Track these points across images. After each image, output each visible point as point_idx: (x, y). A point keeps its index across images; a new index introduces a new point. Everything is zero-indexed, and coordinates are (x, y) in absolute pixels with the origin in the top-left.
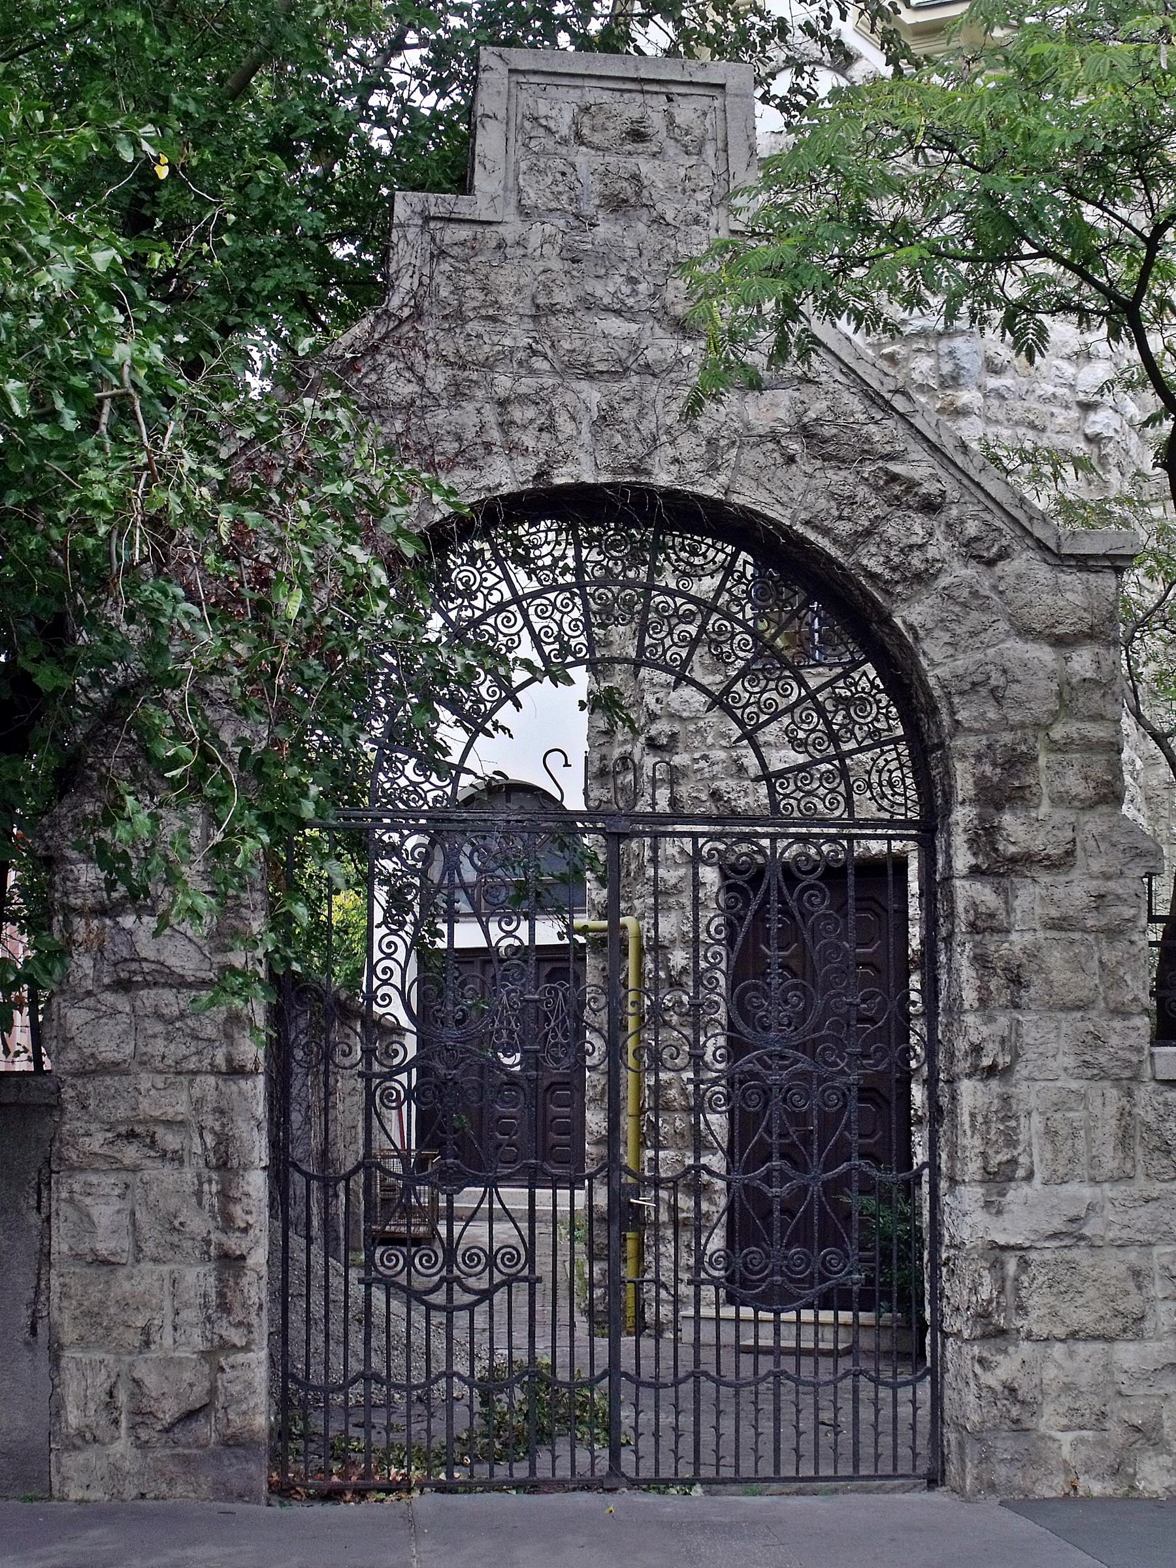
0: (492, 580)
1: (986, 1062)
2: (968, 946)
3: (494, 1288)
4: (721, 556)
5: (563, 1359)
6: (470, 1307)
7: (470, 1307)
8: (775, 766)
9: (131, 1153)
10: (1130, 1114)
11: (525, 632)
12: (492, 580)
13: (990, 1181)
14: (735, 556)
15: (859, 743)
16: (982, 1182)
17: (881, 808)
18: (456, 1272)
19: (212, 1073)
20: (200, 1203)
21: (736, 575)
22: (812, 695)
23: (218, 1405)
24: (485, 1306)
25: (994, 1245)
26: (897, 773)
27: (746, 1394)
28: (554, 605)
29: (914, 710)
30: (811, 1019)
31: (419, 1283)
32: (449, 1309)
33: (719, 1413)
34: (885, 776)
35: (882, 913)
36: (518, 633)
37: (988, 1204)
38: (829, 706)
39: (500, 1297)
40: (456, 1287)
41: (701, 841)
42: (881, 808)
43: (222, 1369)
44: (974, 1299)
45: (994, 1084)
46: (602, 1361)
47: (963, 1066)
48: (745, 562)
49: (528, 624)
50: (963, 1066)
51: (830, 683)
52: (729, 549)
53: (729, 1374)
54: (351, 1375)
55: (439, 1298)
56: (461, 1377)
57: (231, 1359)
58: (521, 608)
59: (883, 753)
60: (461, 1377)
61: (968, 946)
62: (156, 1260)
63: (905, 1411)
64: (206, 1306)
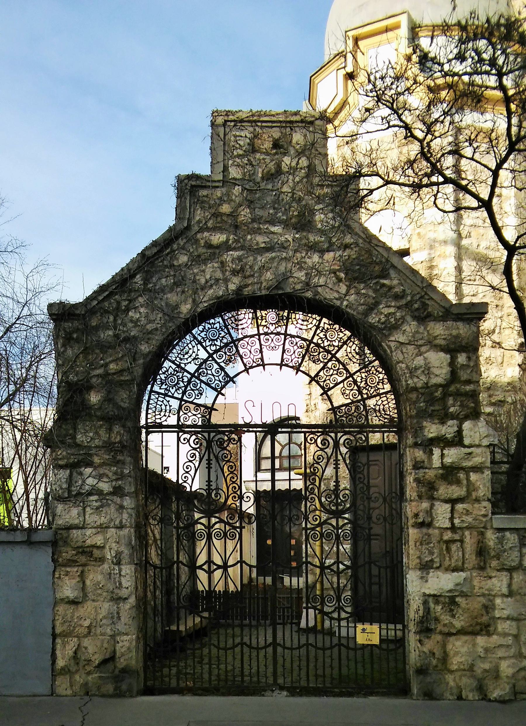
0: (223, 334)
1: (420, 520)
2: (413, 474)
4: (315, 321)
9: (83, 559)
10: (482, 542)
12: (223, 334)
13: (423, 568)
14: (320, 321)
16: (420, 569)
19: (114, 528)
20: (110, 578)
21: (321, 329)
23: (117, 657)
25: (424, 594)
26: (387, 406)
27: (262, 653)
29: (394, 381)
31: (326, 609)
32: (339, 619)
34: (163, 414)
35: (377, 462)
37: (422, 578)
41: (307, 434)
43: (118, 642)
44: (416, 616)
45: (424, 530)
46: (270, 640)
47: (411, 522)
48: (325, 323)
50: (411, 522)
52: (318, 318)
53: (320, 645)
54: (333, 644)
55: (335, 615)
56: (214, 645)
57: (122, 638)
58: (235, 344)
59: (381, 398)
60: (214, 645)
61: (413, 474)
62: (93, 601)
63: (328, 660)
64: (112, 618)
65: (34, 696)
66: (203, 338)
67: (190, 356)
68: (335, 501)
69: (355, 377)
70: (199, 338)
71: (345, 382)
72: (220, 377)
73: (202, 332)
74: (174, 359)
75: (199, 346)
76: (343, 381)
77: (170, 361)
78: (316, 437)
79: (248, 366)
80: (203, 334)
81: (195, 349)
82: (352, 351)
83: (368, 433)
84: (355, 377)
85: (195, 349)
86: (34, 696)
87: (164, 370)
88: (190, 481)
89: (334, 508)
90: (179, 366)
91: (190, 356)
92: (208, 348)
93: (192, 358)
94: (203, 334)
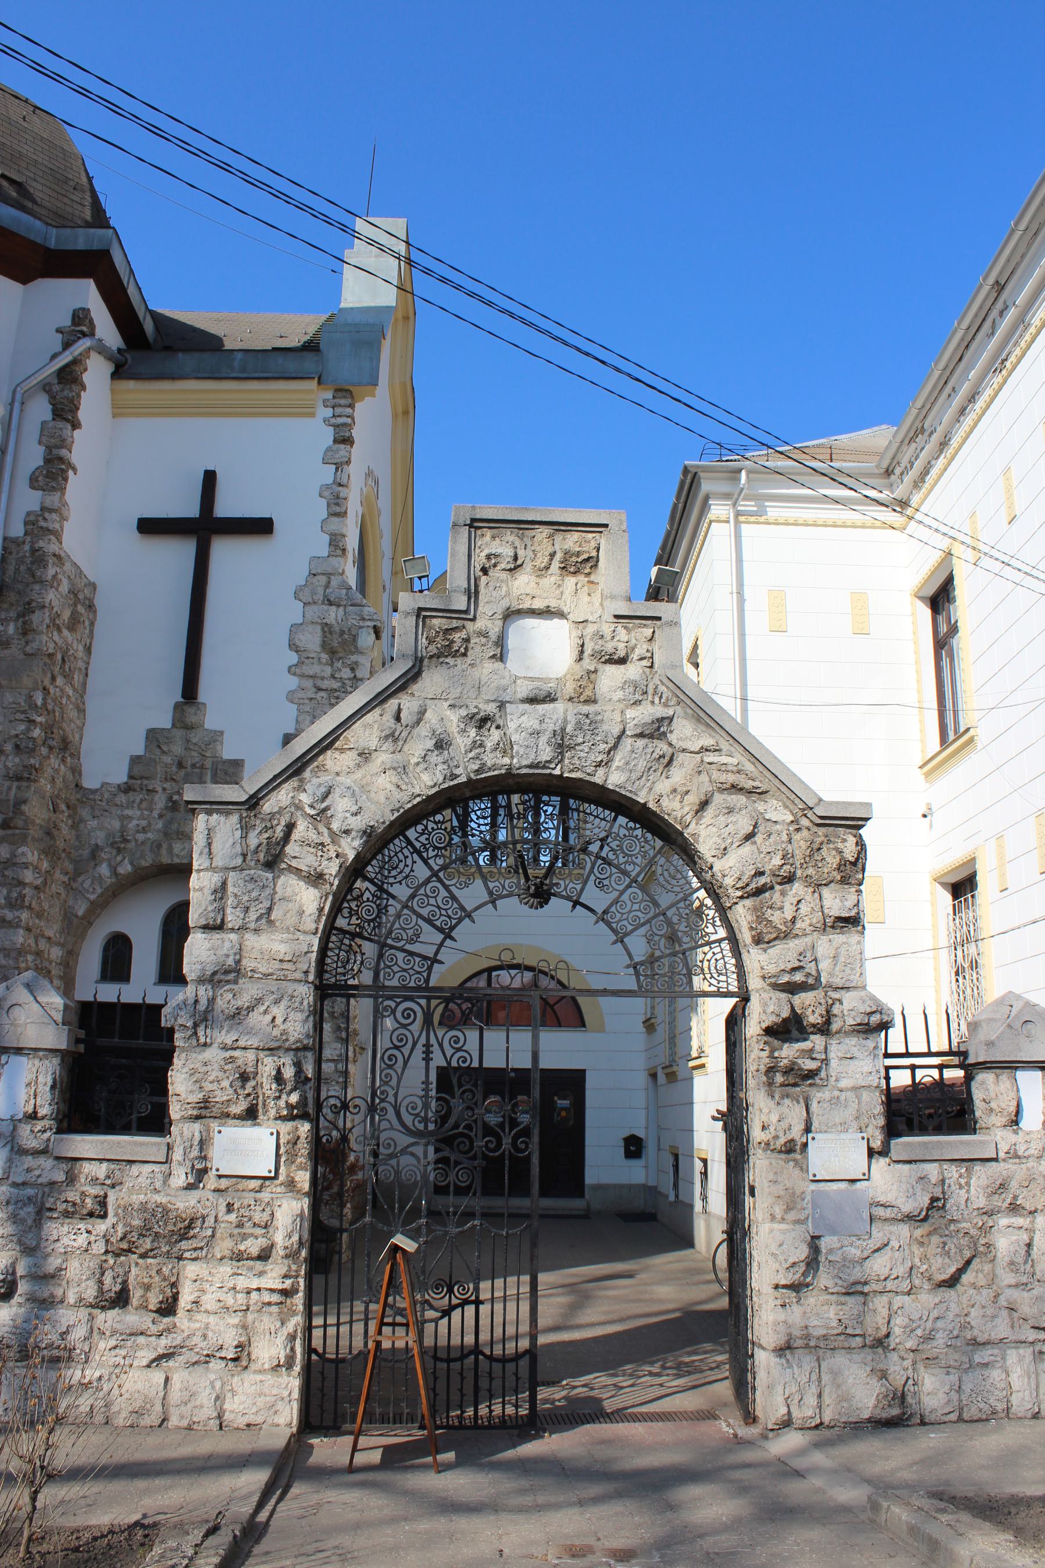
3: (452, 1308)
5: (331, 1342)
6: (436, 1321)
7: (436, 1321)
8: (439, 937)
11: (420, 922)
15: (388, 900)
17: (360, 946)
18: (427, 1297)
22: (598, 857)
24: (446, 1319)
28: (427, 896)
30: (451, 1121)
33: (322, 1390)
36: (416, 924)
38: (611, 856)
39: (456, 1315)
40: (426, 1307)
42: (360, 946)
49: (419, 916)
51: (425, 861)
54: (465, 1352)
65: (946, 383)
66: (424, 845)
67: (401, 872)
68: (422, 1114)
69: (436, 868)
70: (418, 845)
71: (447, 883)
72: (625, 923)
73: (422, 834)
74: (373, 876)
75: (415, 855)
76: (446, 887)
77: (723, 939)
78: (393, 1004)
79: (608, 917)
80: (423, 839)
81: (409, 861)
82: (713, 961)
83: (349, 997)
84: (436, 868)
85: (409, 861)
86: (946, 383)
87: (355, 893)
88: (394, 1083)
89: (421, 1127)
90: (381, 889)
91: (401, 872)
92: (431, 862)
93: (404, 875)
94: (423, 839)
